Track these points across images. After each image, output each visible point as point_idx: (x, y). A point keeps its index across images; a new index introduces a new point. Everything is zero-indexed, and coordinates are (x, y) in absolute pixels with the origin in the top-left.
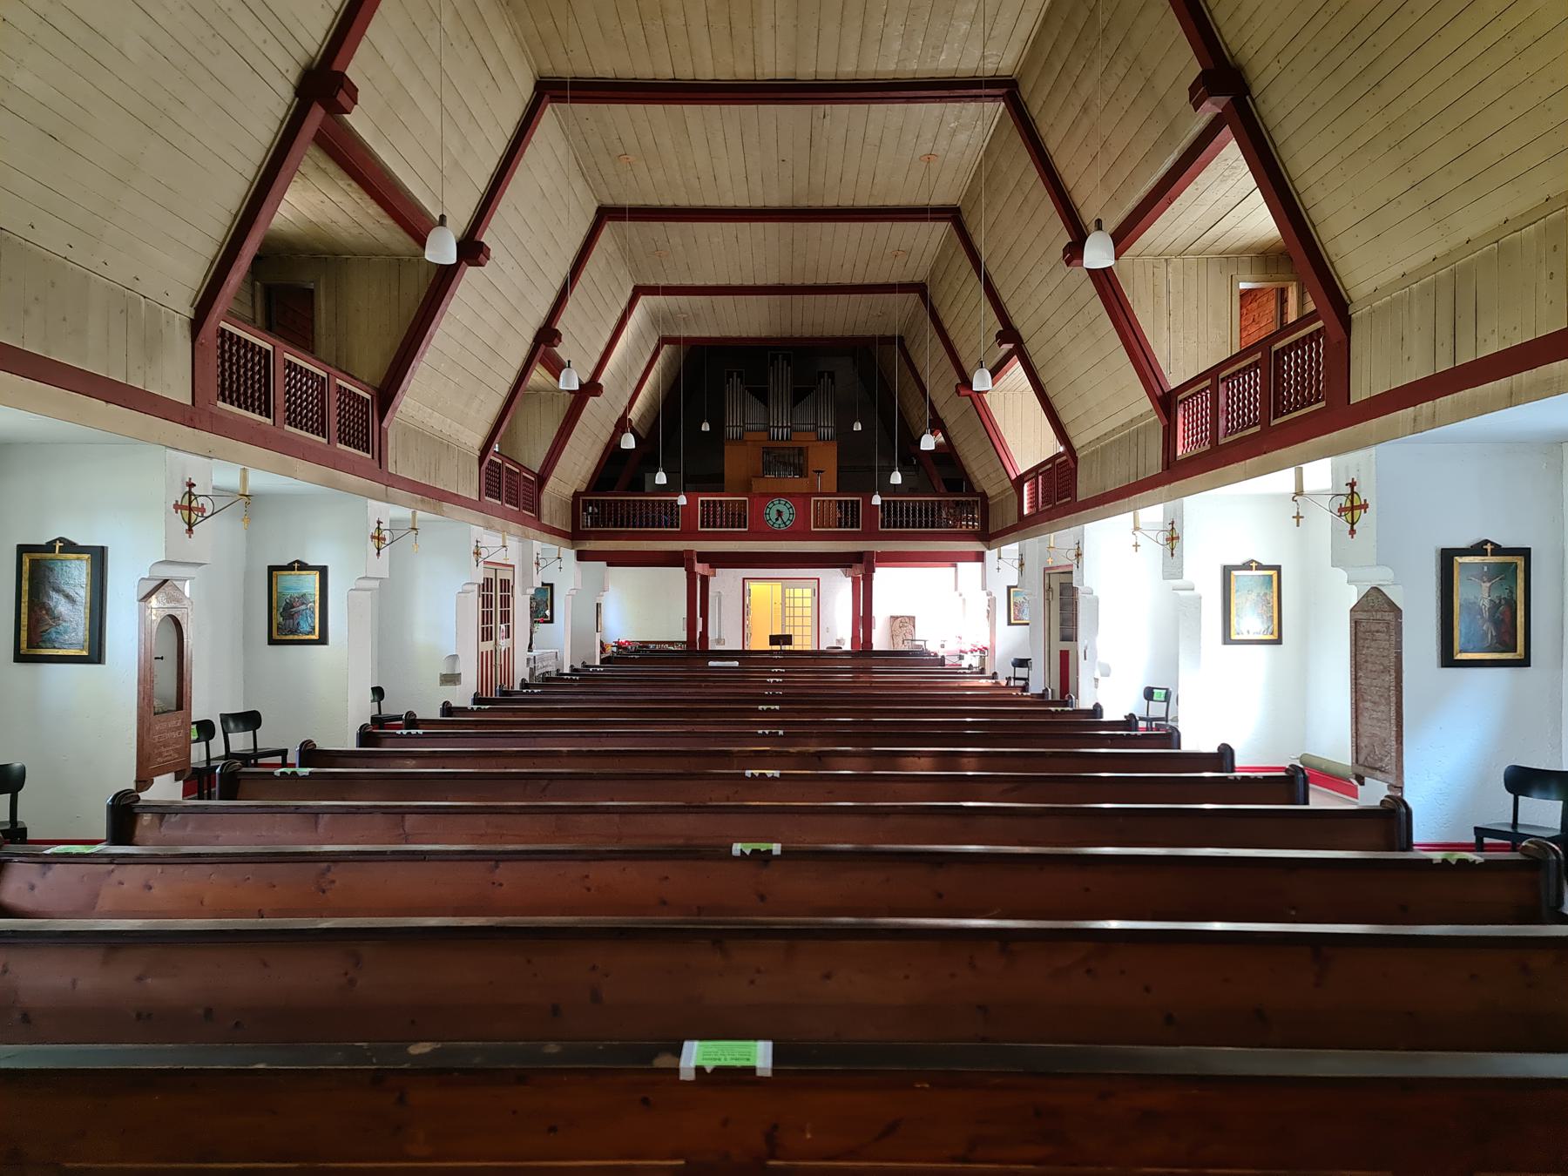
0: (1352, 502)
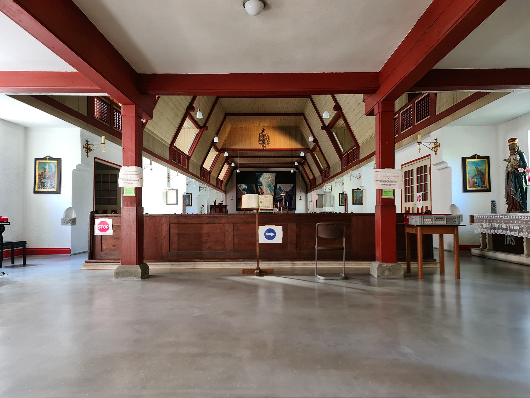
0: (436, 145)
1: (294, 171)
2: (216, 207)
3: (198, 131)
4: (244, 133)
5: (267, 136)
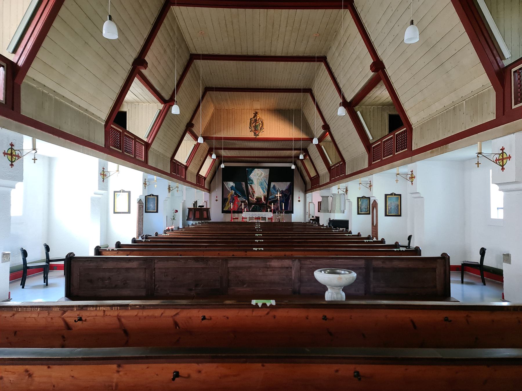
0: (503, 156)
1: (225, 166)
2: (196, 210)
3: (161, 106)
4: (231, 117)
5: (261, 121)
